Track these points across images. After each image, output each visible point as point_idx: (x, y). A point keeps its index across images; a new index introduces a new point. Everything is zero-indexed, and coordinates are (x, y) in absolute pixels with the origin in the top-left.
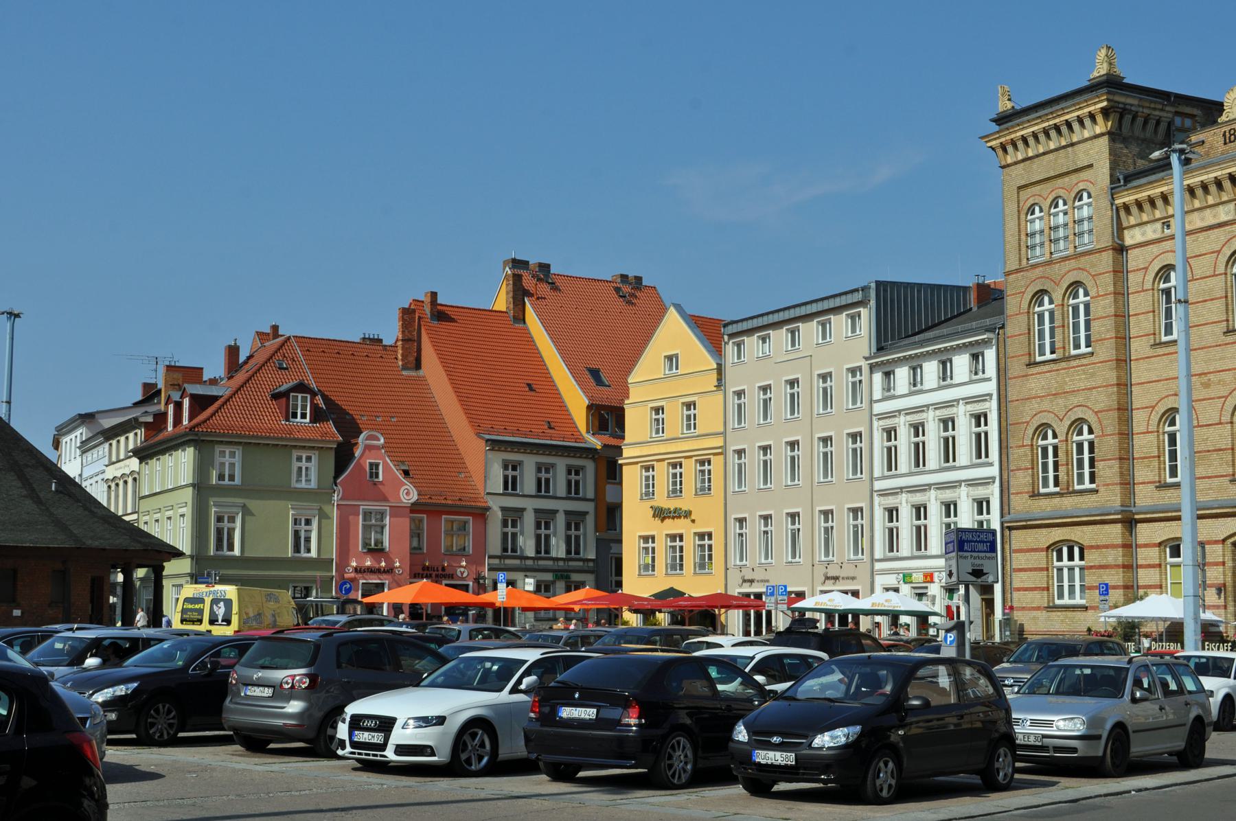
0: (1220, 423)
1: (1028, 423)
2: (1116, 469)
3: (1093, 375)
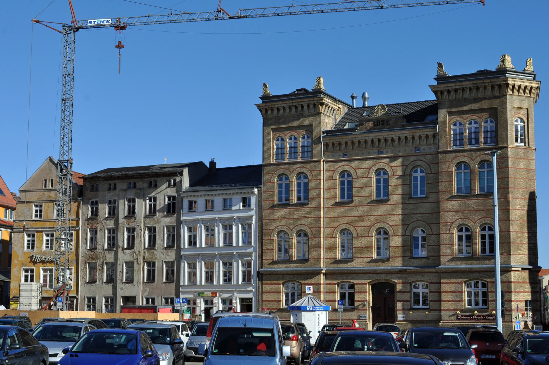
0: (368, 236)
1: (273, 230)
2: (354, 193)
3: (309, 212)
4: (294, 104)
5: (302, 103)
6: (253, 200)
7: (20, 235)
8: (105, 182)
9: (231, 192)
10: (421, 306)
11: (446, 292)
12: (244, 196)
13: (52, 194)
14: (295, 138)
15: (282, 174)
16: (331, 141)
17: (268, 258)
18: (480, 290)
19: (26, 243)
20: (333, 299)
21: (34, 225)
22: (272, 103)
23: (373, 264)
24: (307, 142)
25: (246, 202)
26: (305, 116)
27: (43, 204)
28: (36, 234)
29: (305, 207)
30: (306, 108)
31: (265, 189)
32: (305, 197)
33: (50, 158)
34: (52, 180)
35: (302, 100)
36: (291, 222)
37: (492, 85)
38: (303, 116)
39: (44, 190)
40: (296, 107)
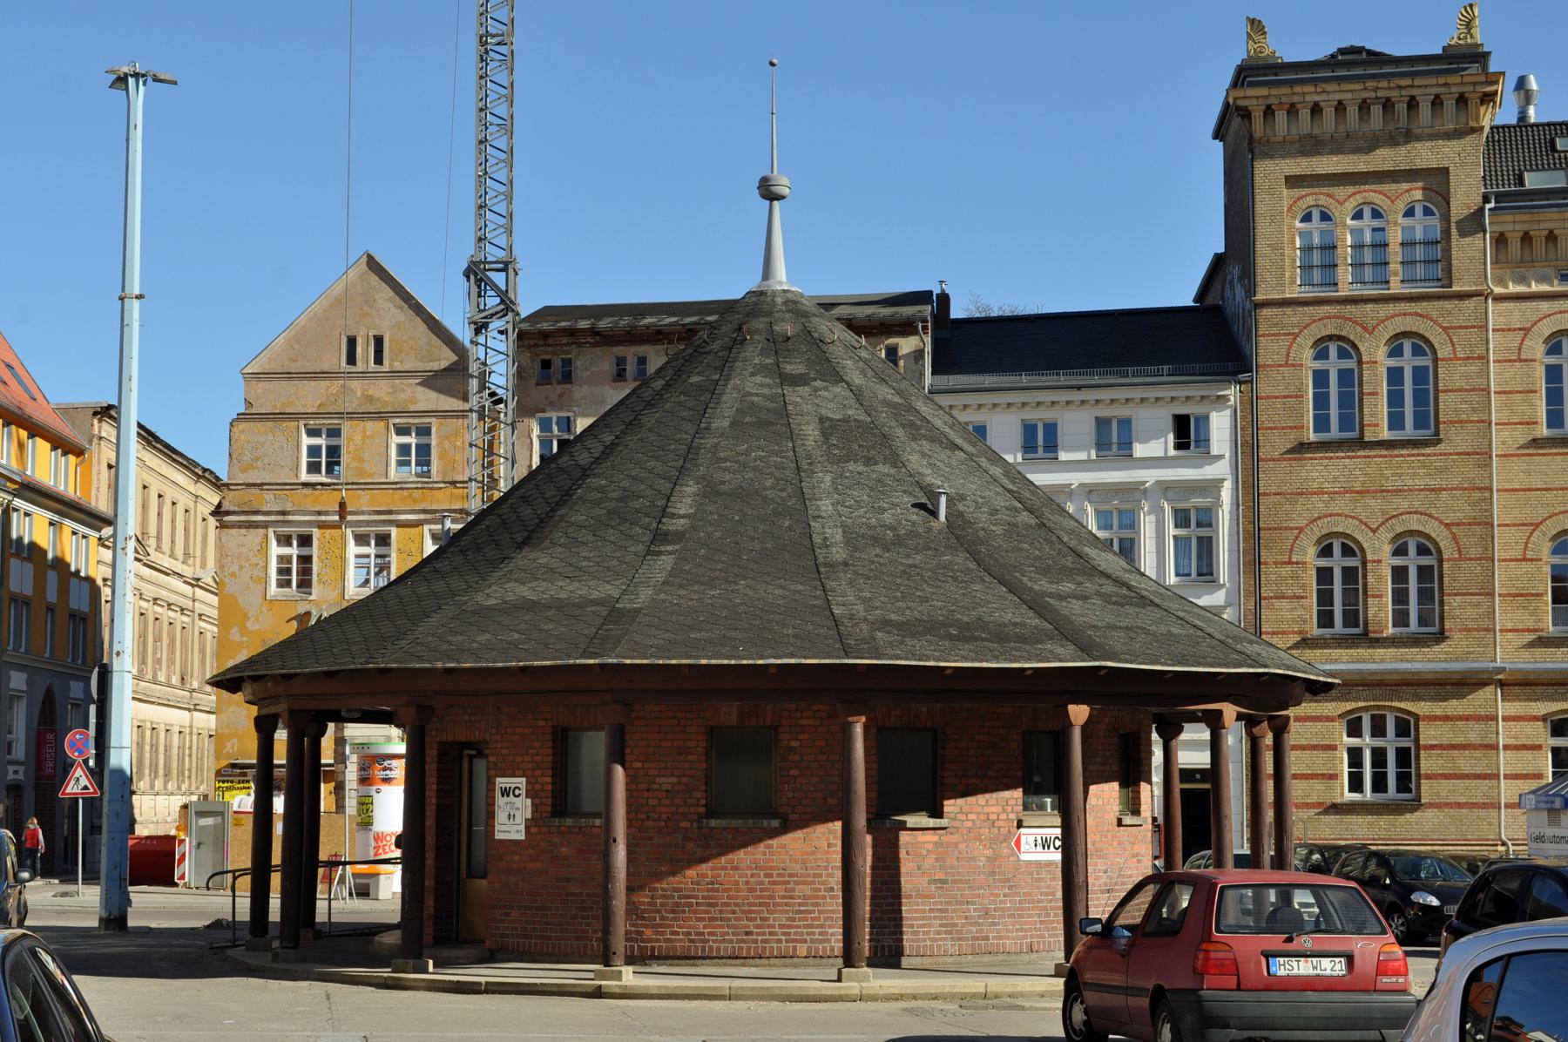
1: (1301, 530)
3: (1440, 470)
4: (1380, 94)
5: (1414, 92)
6: (1220, 427)
7: (255, 536)
8: (599, 351)
9: (1136, 393)
10: (1368, 794)
11: (1303, 748)
12: (1182, 410)
13: (382, 391)
14: (1376, 214)
15: (1331, 338)
16: (1518, 227)
17: (1284, 627)
18: (1391, 743)
19: (273, 566)
20: (1530, 770)
21: (307, 499)
22: (1298, 89)
23: (1539, 652)
24: (1422, 227)
25: (1186, 433)
26: (1419, 138)
27: (346, 427)
28: (394, 531)
29: (1428, 450)
30: (1425, 108)
31: (1264, 387)
32: (1423, 420)
33: (369, 256)
34: (379, 341)
35: (1417, 82)
36: (1372, 503)
37: (1340, 102)
38: (1409, 137)
39: (350, 376)
40: (1388, 105)
